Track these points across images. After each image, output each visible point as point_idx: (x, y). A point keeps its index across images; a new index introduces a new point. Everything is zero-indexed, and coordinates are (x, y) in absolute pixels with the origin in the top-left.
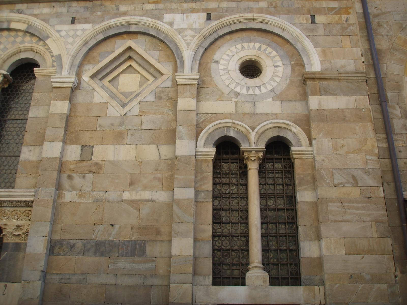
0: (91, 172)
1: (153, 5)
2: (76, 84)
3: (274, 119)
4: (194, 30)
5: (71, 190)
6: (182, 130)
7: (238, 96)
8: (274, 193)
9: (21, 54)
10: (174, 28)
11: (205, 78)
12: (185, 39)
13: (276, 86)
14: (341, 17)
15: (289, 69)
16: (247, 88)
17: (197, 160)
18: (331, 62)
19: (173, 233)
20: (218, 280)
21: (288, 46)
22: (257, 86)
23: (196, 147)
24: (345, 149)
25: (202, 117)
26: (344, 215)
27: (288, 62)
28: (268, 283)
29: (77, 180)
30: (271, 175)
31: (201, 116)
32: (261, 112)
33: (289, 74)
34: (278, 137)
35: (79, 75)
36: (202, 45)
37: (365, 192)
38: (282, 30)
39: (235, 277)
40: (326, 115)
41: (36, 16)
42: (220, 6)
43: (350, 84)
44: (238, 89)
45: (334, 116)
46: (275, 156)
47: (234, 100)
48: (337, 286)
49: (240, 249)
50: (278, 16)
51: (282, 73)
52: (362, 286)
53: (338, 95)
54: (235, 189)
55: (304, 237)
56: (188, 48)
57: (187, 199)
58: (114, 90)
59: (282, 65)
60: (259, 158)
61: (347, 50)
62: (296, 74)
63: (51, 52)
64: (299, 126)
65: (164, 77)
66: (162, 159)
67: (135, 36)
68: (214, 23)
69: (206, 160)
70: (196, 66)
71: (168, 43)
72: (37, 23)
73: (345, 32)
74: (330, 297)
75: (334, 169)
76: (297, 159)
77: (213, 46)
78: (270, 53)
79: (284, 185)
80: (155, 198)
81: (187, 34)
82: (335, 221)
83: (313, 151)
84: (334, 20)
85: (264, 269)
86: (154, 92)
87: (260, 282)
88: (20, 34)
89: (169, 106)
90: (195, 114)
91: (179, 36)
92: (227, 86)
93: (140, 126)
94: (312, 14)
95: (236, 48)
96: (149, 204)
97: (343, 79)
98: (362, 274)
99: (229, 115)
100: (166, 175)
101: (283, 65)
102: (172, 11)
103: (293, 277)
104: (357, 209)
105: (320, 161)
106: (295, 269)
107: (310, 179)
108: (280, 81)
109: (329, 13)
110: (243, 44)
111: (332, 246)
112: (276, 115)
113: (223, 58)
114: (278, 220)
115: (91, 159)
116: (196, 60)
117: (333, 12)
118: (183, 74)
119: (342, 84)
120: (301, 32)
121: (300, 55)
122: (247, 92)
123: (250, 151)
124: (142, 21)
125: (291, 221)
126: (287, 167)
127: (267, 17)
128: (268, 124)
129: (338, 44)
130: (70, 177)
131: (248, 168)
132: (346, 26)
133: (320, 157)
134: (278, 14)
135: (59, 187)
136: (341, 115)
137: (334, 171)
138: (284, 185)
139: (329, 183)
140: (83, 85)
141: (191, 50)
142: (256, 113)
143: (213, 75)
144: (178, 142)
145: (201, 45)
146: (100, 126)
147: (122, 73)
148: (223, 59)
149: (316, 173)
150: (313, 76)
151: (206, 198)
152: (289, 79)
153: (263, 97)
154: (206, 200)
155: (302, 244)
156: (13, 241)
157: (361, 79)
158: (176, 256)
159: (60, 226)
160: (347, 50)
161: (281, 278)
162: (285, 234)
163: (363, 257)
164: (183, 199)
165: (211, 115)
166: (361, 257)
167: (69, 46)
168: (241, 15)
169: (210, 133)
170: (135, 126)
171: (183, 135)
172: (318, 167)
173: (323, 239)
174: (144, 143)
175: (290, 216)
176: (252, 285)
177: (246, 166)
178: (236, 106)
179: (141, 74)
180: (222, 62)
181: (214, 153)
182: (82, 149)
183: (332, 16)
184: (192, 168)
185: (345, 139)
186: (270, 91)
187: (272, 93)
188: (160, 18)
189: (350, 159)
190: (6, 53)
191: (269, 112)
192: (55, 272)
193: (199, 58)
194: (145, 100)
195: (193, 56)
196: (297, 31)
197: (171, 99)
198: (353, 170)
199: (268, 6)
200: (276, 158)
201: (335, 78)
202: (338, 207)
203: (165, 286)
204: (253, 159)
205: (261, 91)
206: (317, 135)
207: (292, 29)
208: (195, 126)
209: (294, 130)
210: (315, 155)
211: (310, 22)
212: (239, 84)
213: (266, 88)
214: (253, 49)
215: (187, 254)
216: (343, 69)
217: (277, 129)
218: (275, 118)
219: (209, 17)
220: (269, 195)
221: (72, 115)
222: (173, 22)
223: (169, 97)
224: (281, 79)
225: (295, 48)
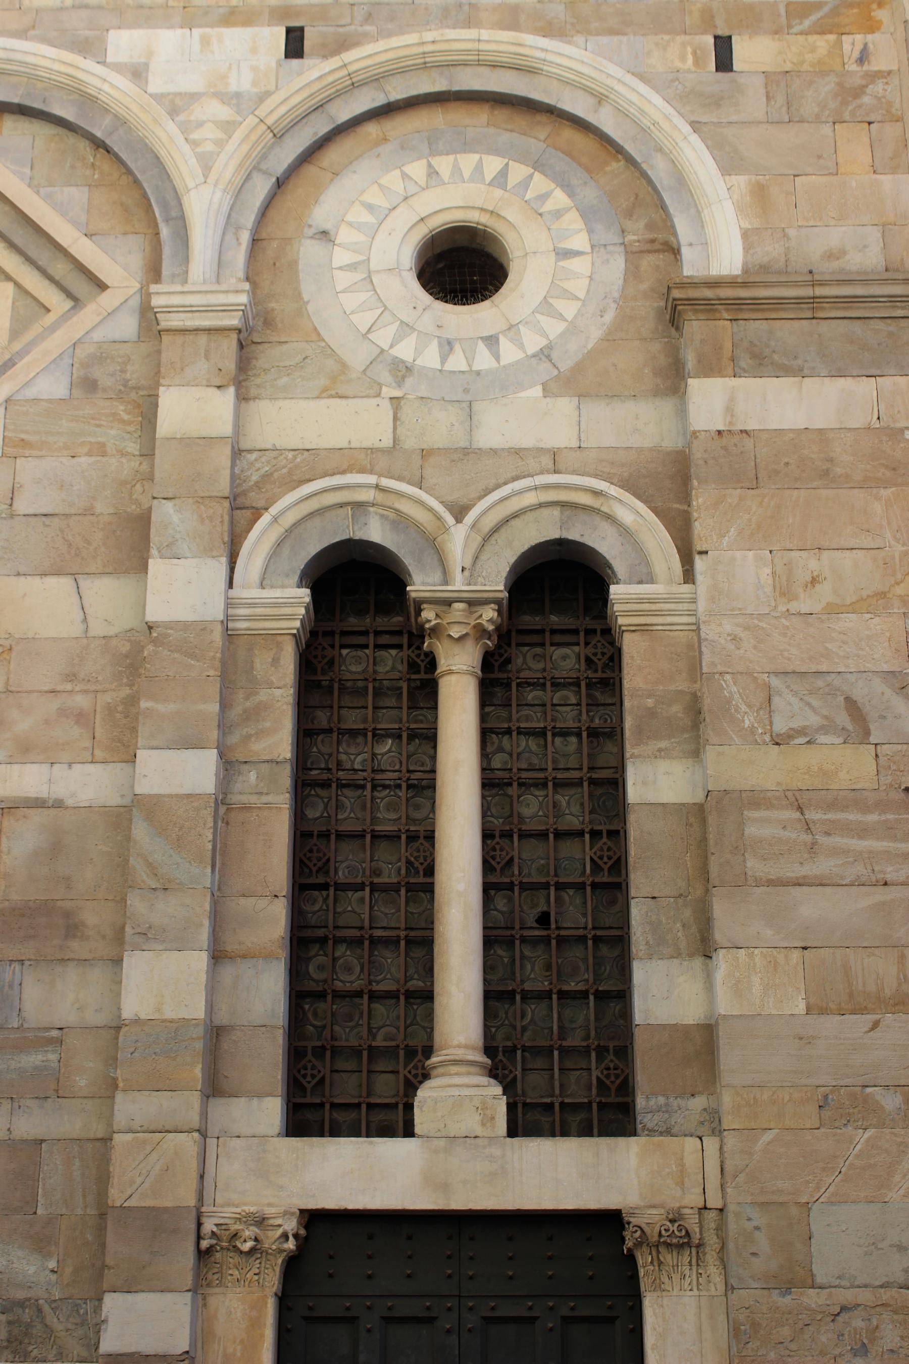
3: (548, 472)
4: (234, 99)
6: (175, 519)
7: (403, 377)
8: (541, 770)
10: (153, 88)
11: (273, 305)
12: (193, 136)
13: (562, 335)
14: (839, 43)
15: (618, 264)
16: (440, 345)
17: (230, 636)
18: (785, 236)
19: (128, 930)
20: (309, 1115)
21: (617, 166)
22: (485, 335)
23: (231, 585)
24: (825, 592)
25: (258, 465)
26: (806, 856)
27: (612, 237)
30: (532, 695)
31: (256, 460)
32: (495, 446)
33: (661, 256)
37: (894, 767)
38: (591, 101)
39: (379, 1101)
40: (752, 455)
43: (857, 326)
44: (405, 351)
45: (786, 460)
46: (554, 618)
47: (387, 392)
48: (768, 1136)
49: (402, 991)
50: (580, 39)
51: (587, 281)
52: (867, 1135)
53: (806, 371)
54: (390, 751)
55: (647, 943)
56: (206, 177)
57: (189, 796)
59: (588, 249)
61: (854, 184)
62: (644, 286)
64: (644, 501)
65: (107, 300)
66: (91, 633)
69: (272, 637)
70: (239, 256)
71: (124, 156)
73: (850, 108)
74: (741, 1178)
75: (777, 674)
76: (633, 634)
77: (310, 170)
78: (544, 197)
79: (584, 734)
80: (60, 791)
81: (205, 118)
82: (771, 883)
83: (694, 601)
84: (809, 57)
85: (493, 1073)
86: (68, 361)
87: (470, 1122)
89: (126, 417)
90: (228, 451)
91: (171, 127)
92: (365, 336)
93: (9, 501)
94: (720, 32)
95: (405, 176)
96: (38, 817)
97: (832, 308)
98: (869, 1090)
99: (367, 455)
100: (108, 698)
101: (593, 247)
103: (609, 1100)
104: (863, 832)
105: (722, 641)
106: (615, 1069)
107: (680, 715)
108: (579, 314)
109: (790, 26)
110: (436, 161)
111: (756, 980)
112: (555, 454)
113: (349, 218)
114: (556, 875)
116: (238, 228)
117: (807, 23)
118: (179, 288)
119: (824, 326)
120: (669, 110)
121: (663, 207)
122: (444, 359)
123: (448, 603)
124: (18, 56)
125: (606, 879)
126: (600, 665)
129: (819, 157)
131: (438, 671)
132: (858, 81)
133: (720, 625)
134: (578, 32)
136: (813, 456)
137: (775, 682)
138: (584, 734)
139: (752, 730)
141: (215, 186)
142: (473, 447)
143: (307, 289)
144: (155, 565)
145: (259, 163)
148: (351, 224)
149: (705, 689)
150: (708, 293)
151: (265, 791)
152: (614, 306)
154: (265, 799)
157: (903, 308)
158: (137, 1021)
160: (854, 184)
161: (562, 1104)
162: (581, 932)
163: (876, 1025)
164: (170, 796)
165: (295, 457)
166: (870, 1025)
168: (429, 36)
169: (289, 531)
171: (178, 536)
172: (713, 664)
173: (722, 952)
174: (22, 569)
175: (605, 859)
176: (438, 1134)
177: (432, 663)
178: (396, 419)
179: (17, 285)
180: (344, 235)
181: (302, 611)
183: (801, 38)
184: (212, 673)
185: (826, 554)
186: (534, 356)
187: (545, 366)
189: (840, 633)
191: (527, 442)
193: (249, 219)
194: (31, 393)
195: (225, 209)
197: (136, 388)
198: (852, 678)
200: (555, 627)
201: (799, 301)
202: (784, 827)
203: (98, 1139)
204: (455, 632)
205: (497, 358)
206: (715, 537)
207: (634, 98)
208: (226, 504)
209: (625, 516)
210: (703, 618)
211: (712, 66)
212: (413, 329)
213: (521, 346)
214: (471, 180)
215: (185, 1014)
216: (835, 265)
217: (556, 512)
218: (550, 466)
220: (524, 775)
222: (146, 65)
223: (125, 383)
224: (583, 305)
225: (644, 175)
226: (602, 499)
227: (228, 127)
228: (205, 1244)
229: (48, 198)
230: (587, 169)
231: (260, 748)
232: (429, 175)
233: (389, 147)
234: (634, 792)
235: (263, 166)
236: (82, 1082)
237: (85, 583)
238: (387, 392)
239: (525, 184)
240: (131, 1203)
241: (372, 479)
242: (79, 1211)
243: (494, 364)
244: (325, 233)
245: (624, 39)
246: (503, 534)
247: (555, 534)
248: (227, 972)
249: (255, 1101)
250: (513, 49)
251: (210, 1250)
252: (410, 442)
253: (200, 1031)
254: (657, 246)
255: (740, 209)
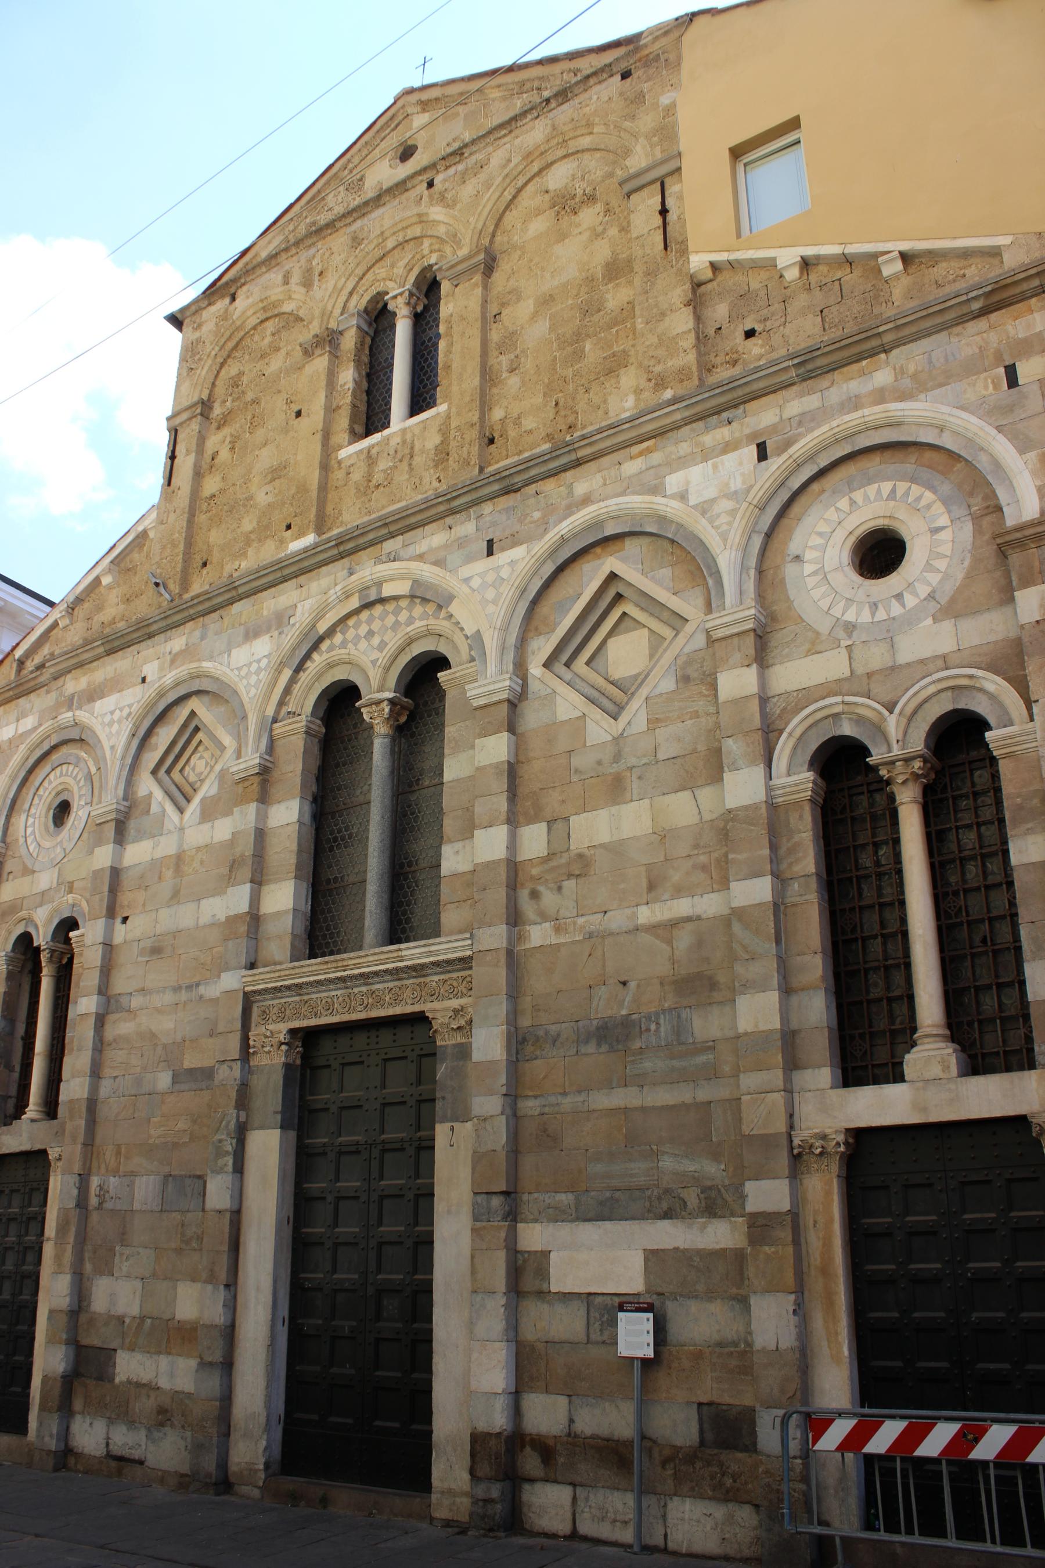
0: (570, 876)
1: (640, 460)
2: (519, 689)
4: (734, 496)
5: (539, 920)
6: (734, 748)
7: (852, 632)
9: (413, 645)
10: (691, 504)
11: (774, 608)
13: (941, 580)
15: (969, 527)
16: (870, 607)
19: (737, 984)
28: (954, 1070)
29: (549, 898)
34: (955, 711)
35: (520, 668)
36: (757, 529)
38: (937, 431)
41: (420, 557)
42: (785, 416)
44: (850, 616)
50: (922, 396)
51: (951, 544)
58: (600, 682)
60: (916, 776)
63: (462, 629)
66: (704, 820)
67: (618, 545)
68: (775, 464)
69: (797, 804)
70: (750, 586)
71: (684, 544)
72: (427, 572)
77: (785, 522)
78: (919, 499)
80: (698, 911)
85: (953, 1038)
87: (936, 1071)
88: (404, 603)
89: (706, 693)
91: (704, 522)
92: (827, 613)
94: (1007, 364)
95: (837, 509)
96: (689, 926)
100: (715, 855)
101: (952, 521)
102: (683, 462)
108: (949, 566)
110: (853, 495)
112: (944, 657)
113: (810, 544)
115: (568, 849)
116: (748, 569)
122: (873, 615)
123: (893, 763)
124: (624, 506)
127: (895, 409)
128: (926, 687)
130: (535, 895)
135: (514, 918)
140: (534, 686)
143: (792, 593)
144: (727, 776)
146: (576, 771)
147: (611, 634)
150: (1018, 535)
153: (910, 620)
154: (804, 898)
155: (1028, 969)
156: (454, 1042)
158: (746, 1034)
159: (528, 999)
164: (749, 906)
167: (491, 608)
168: (834, 424)
169: (800, 739)
170: (645, 756)
178: (850, 658)
180: (809, 555)
182: (549, 829)
184: (763, 832)
186: (925, 599)
187: (933, 603)
188: (656, 489)
190: (384, 653)
191: (927, 654)
192: (531, 1094)
193: (753, 562)
194: (658, 691)
196: (973, 424)
199: (896, 377)
205: (904, 606)
207: (959, 422)
209: (990, 687)
213: (917, 595)
214: (876, 500)
217: (949, 693)
219: (762, 454)
221: (522, 758)
222: (687, 490)
226: (975, 680)
227: (733, 513)
228: (795, 1151)
229: (653, 579)
230: (942, 473)
231: (797, 869)
232: (851, 505)
233: (826, 495)
234: (1014, 860)
235: (757, 529)
236: (727, 1068)
237: (697, 792)
238: (844, 643)
239: (907, 493)
240: (754, 1132)
241: (839, 699)
242: (733, 1138)
243: (902, 610)
244: (797, 557)
245: (949, 387)
246: (920, 713)
247: (950, 707)
248: (794, 1000)
249: (817, 1070)
250: (884, 415)
251: (800, 1154)
252: (860, 670)
253: (778, 1036)
254: (991, 510)
255: (1034, 473)
